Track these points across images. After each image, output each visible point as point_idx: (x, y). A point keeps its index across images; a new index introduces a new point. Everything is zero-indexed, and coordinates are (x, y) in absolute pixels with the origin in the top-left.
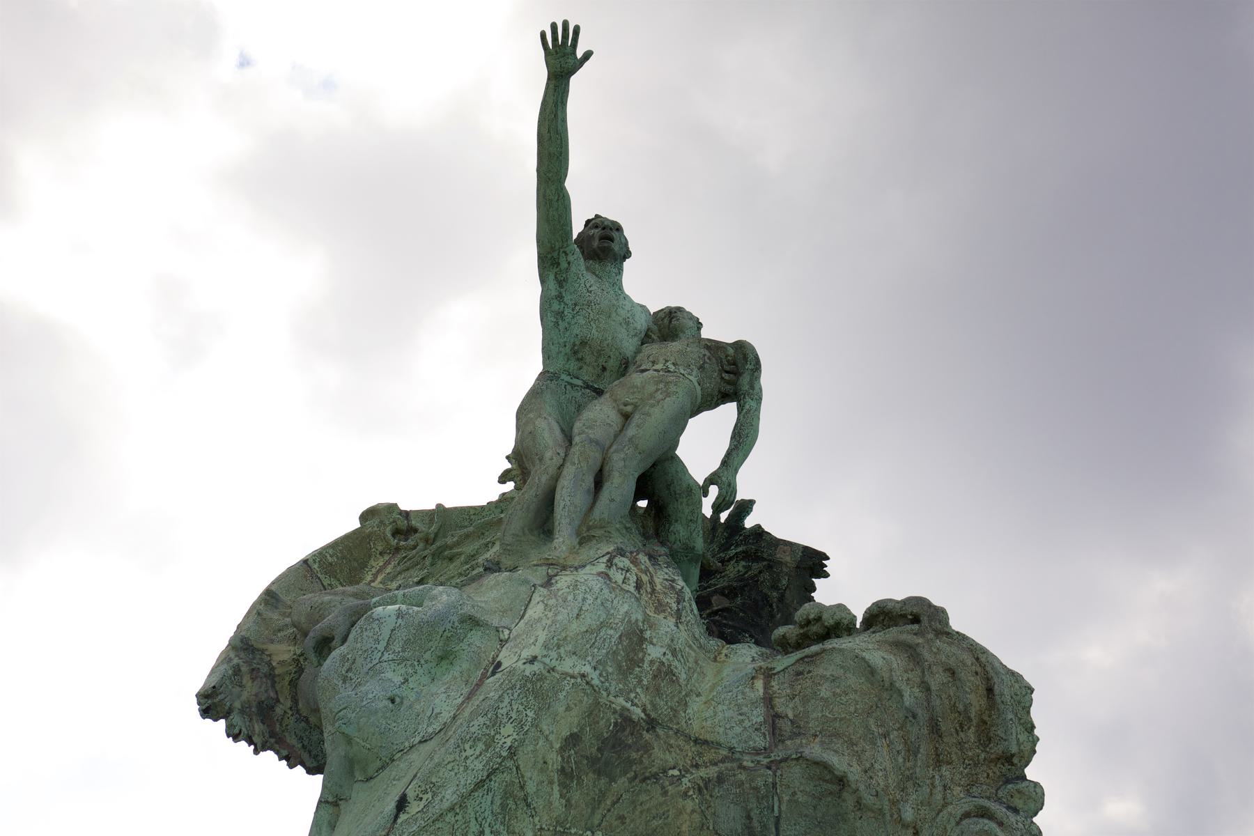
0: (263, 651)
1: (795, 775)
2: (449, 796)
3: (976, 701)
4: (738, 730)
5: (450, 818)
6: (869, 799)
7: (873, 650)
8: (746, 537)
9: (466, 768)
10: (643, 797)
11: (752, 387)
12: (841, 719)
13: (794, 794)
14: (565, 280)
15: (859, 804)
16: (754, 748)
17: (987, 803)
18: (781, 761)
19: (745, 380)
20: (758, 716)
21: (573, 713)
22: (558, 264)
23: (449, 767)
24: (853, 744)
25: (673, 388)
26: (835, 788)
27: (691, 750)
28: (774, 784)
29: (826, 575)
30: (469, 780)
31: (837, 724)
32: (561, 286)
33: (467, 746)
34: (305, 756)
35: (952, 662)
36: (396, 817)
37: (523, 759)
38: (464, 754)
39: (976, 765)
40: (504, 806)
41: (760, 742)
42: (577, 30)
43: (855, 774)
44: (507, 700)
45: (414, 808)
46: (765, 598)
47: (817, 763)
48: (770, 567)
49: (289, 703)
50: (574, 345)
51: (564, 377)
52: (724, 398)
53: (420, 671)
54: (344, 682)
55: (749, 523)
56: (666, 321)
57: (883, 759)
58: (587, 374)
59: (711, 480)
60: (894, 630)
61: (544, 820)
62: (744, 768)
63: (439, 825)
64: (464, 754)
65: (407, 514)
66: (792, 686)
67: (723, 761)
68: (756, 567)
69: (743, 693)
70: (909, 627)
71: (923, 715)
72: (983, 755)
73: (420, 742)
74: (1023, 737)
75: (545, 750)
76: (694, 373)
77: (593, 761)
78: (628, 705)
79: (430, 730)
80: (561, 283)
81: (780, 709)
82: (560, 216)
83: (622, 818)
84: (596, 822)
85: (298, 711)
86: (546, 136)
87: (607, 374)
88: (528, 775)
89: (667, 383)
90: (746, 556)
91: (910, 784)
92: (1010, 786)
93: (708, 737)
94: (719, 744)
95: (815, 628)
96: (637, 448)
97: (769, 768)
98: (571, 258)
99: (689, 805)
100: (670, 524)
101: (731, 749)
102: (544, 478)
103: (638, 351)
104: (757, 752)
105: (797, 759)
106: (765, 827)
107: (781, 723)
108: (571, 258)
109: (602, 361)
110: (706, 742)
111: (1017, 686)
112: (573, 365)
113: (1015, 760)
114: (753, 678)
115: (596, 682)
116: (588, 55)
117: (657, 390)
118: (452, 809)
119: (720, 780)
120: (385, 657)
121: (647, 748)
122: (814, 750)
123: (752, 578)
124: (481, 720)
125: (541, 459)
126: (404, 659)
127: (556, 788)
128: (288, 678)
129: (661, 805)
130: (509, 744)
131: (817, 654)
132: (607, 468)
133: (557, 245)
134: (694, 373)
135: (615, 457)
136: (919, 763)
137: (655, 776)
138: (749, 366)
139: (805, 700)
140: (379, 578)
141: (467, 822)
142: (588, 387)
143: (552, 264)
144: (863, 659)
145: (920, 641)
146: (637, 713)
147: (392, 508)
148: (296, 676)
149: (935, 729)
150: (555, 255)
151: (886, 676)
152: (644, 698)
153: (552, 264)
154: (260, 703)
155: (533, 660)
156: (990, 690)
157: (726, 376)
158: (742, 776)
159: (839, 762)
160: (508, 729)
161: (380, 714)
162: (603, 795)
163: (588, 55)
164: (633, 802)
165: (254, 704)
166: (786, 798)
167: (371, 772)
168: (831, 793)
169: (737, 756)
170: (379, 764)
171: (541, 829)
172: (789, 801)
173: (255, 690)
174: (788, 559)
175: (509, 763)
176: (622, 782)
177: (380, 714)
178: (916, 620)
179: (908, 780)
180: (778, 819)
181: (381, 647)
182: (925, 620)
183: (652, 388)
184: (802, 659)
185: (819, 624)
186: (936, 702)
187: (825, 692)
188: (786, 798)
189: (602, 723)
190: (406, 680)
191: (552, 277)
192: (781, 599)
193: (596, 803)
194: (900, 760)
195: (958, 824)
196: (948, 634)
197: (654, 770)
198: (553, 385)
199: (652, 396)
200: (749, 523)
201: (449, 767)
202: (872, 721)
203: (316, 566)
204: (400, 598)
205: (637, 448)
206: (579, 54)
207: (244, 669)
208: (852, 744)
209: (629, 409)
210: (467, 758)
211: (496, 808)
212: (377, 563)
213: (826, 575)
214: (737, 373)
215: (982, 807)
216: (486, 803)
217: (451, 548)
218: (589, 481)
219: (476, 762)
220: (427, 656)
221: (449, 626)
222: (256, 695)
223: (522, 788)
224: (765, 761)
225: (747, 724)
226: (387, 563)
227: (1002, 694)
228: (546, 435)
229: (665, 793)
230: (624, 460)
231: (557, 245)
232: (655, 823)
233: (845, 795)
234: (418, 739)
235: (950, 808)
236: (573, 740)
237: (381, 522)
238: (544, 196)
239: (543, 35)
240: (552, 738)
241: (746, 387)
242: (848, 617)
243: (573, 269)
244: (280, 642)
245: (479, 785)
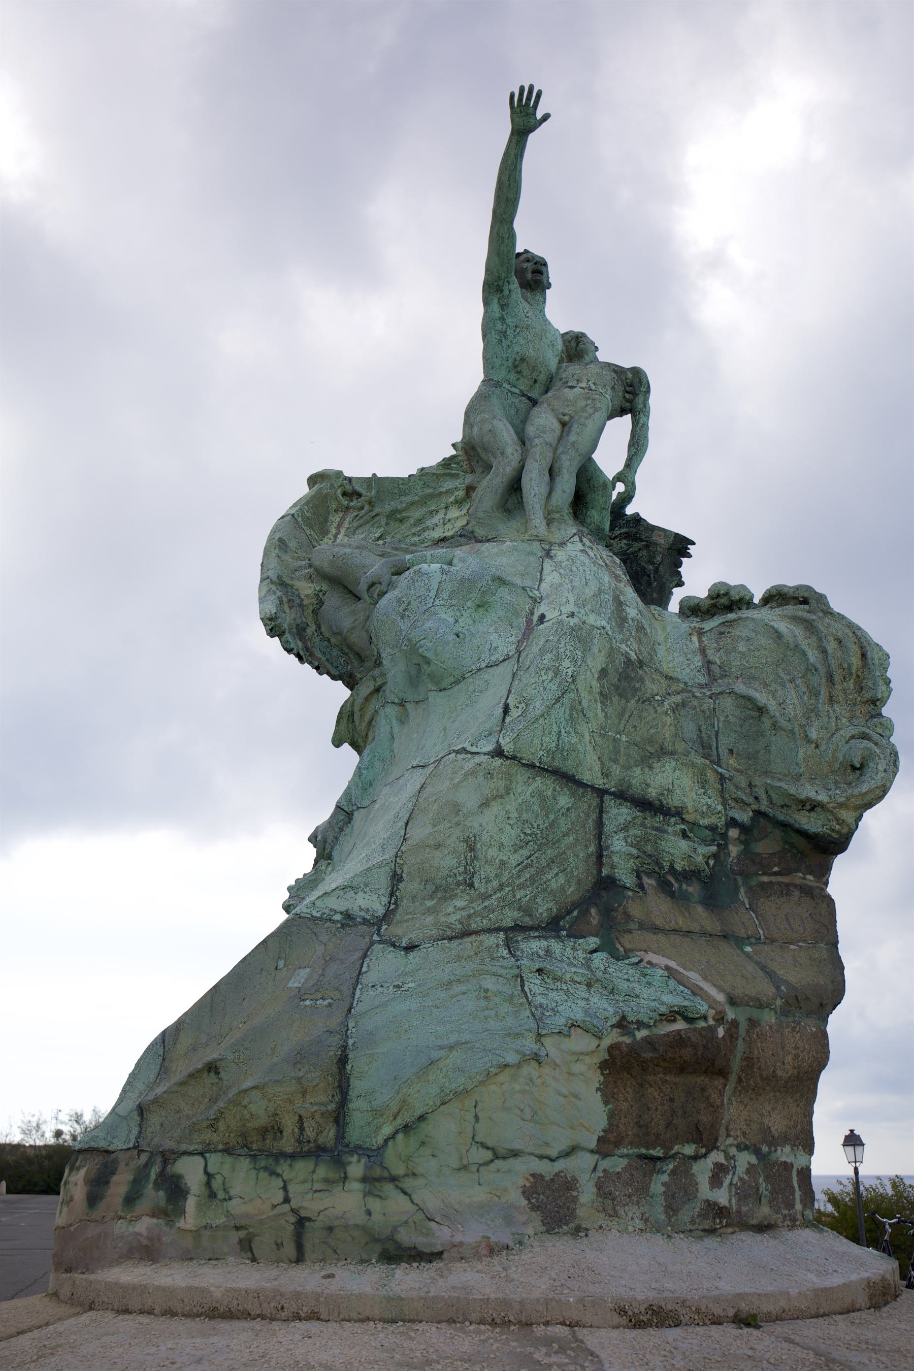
0: (292, 586)
1: (727, 703)
2: (538, 706)
3: (856, 661)
4: (688, 670)
5: (541, 721)
6: (783, 723)
7: (773, 617)
8: (628, 521)
9: (545, 689)
10: (645, 714)
11: (645, 406)
12: (756, 668)
13: (727, 716)
14: (507, 305)
15: (775, 726)
16: (699, 684)
17: (867, 731)
18: (719, 694)
19: (640, 399)
20: (698, 661)
21: (602, 654)
22: (502, 291)
23: (533, 686)
24: (767, 685)
25: (598, 405)
26: (756, 714)
27: (664, 682)
28: (714, 709)
29: (690, 556)
30: (550, 696)
31: (753, 671)
32: (503, 310)
33: (543, 673)
34: (329, 667)
35: (840, 634)
36: (504, 719)
37: (580, 684)
38: (541, 679)
39: (854, 705)
40: (571, 715)
41: (702, 680)
42: (539, 94)
43: (772, 706)
44: (563, 643)
45: (514, 713)
46: (643, 569)
47: (743, 697)
48: (647, 546)
49: (314, 627)
50: (515, 360)
51: (505, 385)
52: (622, 412)
53: (465, 615)
54: (402, 618)
55: (630, 510)
56: (573, 344)
57: (792, 697)
58: (523, 385)
59: (619, 478)
60: (790, 607)
61: (594, 726)
62: (696, 697)
63: (535, 725)
64: (541, 679)
65: (350, 479)
66: (717, 642)
67: (682, 692)
68: (637, 545)
69: (686, 645)
70: (802, 606)
71: (822, 670)
72: (859, 699)
73: (487, 667)
74: (884, 688)
75: (589, 681)
76: (609, 392)
77: (617, 688)
78: (628, 650)
79: (493, 658)
80: (503, 307)
81: (711, 658)
82: (508, 251)
83: (635, 727)
84: (622, 729)
85: (321, 634)
86: (506, 183)
87: (537, 385)
88: (582, 695)
89: (594, 400)
90: (627, 536)
91: (813, 714)
92: (875, 720)
93: (672, 674)
94: (678, 680)
95: (723, 601)
96: (577, 451)
97: (711, 698)
98: (512, 287)
99: (669, 720)
100: (587, 509)
101: (686, 683)
102: (508, 470)
103: (558, 368)
104: (701, 686)
105: (729, 693)
106: (709, 737)
107: (712, 667)
108: (512, 287)
109: (535, 375)
110: (671, 678)
111: (880, 653)
112: (512, 376)
113: (878, 703)
114: (690, 634)
115: (610, 633)
116: (546, 117)
117: (587, 405)
118: (542, 715)
119: (684, 705)
120: (437, 602)
121: (641, 680)
122: (740, 687)
123: (633, 553)
124: (549, 656)
125: (502, 454)
126: (452, 605)
127: (599, 705)
128: (311, 608)
129: (654, 719)
130: (570, 674)
131: (735, 620)
132: (557, 465)
133: (503, 275)
134: (609, 392)
135: (563, 457)
136: (821, 701)
137: (648, 699)
138: (643, 389)
139: (728, 653)
140: (343, 531)
142: (524, 395)
143: (497, 291)
144: (773, 627)
145: (814, 617)
146: (633, 656)
147: (339, 474)
148: (318, 606)
149: (830, 678)
150: (501, 283)
151: (791, 640)
152: (635, 646)
153: (497, 291)
154: (298, 625)
155: (572, 615)
156: (864, 655)
157: (627, 396)
158: (695, 703)
159: (762, 698)
160: (566, 663)
161: (451, 645)
162: (624, 710)
163: (546, 117)
164: (640, 717)
165: (294, 626)
166: (722, 719)
167: (444, 684)
168: (752, 717)
169: (689, 688)
170: (452, 680)
171: (593, 731)
172: (724, 721)
173: (293, 616)
174: (662, 541)
175: (573, 687)
176: (632, 703)
177: (451, 645)
178: (805, 602)
179: (812, 712)
180: (717, 732)
181: (433, 594)
182: (813, 603)
183: (583, 403)
184: (723, 623)
185: (726, 598)
186: (832, 661)
187: (742, 647)
188: (722, 719)
189: (617, 661)
190: (457, 621)
191: (495, 301)
192: (656, 571)
193: (621, 715)
194: (806, 698)
195: (847, 742)
196: (831, 614)
197: (648, 695)
198: (497, 391)
199: (583, 409)
200: (630, 510)
201: (533, 686)
202: (780, 670)
203: (300, 519)
204: (429, 557)
205: (577, 451)
206: (539, 115)
207: (285, 600)
208: (766, 685)
209: (566, 418)
210: (543, 681)
212: (335, 518)
213: (690, 556)
214: (635, 394)
215: (864, 732)
216: (561, 712)
217: (400, 513)
218: (547, 477)
219: (551, 684)
220: (469, 604)
221: (485, 583)
222: (295, 619)
223: (580, 703)
224: (708, 693)
225: (692, 666)
226: (343, 520)
227: (873, 659)
228: (505, 434)
229: (656, 712)
230: (570, 460)
231: (503, 275)
232: (652, 731)
233: (764, 719)
234: (483, 665)
235: (841, 732)
236: (603, 673)
237: (332, 485)
238: (498, 234)
239: (512, 96)
240: (593, 670)
241: (641, 406)
242: (750, 595)
243: (514, 296)
244: (298, 579)
245: (558, 700)
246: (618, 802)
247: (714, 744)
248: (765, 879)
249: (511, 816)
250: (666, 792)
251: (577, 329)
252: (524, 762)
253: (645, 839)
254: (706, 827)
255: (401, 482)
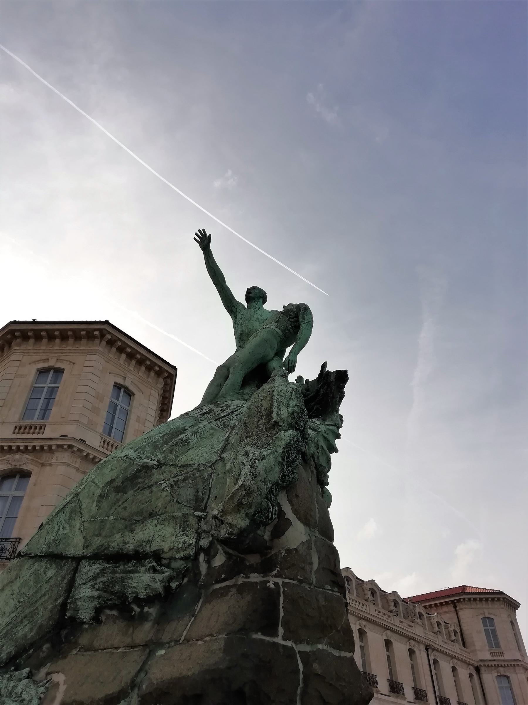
42: (204, 230)
84: (111, 512)
97: (210, 467)
141: (54, 527)
157: (292, 320)
162: (118, 500)
163: (210, 235)
188: (215, 478)
211: (67, 518)
223: (80, 507)
239: (195, 239)
245: (61, 510)
246: (92, 562)
247: (207, 497)
248: (217, 586)
249: (15, 592)
250: (144, 544)
251: (297, 301)
252: (32, 555)
253: (113, 582)
254: (181, 559)
255: (189, 423)
